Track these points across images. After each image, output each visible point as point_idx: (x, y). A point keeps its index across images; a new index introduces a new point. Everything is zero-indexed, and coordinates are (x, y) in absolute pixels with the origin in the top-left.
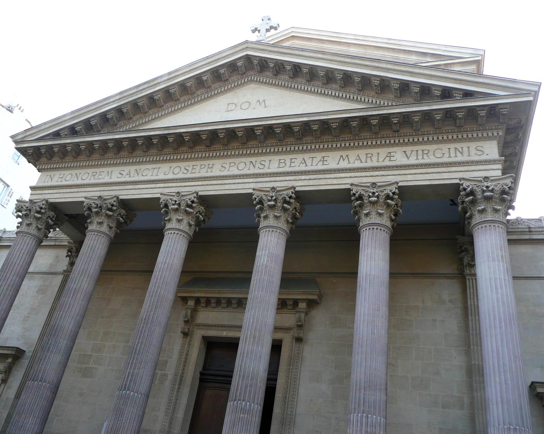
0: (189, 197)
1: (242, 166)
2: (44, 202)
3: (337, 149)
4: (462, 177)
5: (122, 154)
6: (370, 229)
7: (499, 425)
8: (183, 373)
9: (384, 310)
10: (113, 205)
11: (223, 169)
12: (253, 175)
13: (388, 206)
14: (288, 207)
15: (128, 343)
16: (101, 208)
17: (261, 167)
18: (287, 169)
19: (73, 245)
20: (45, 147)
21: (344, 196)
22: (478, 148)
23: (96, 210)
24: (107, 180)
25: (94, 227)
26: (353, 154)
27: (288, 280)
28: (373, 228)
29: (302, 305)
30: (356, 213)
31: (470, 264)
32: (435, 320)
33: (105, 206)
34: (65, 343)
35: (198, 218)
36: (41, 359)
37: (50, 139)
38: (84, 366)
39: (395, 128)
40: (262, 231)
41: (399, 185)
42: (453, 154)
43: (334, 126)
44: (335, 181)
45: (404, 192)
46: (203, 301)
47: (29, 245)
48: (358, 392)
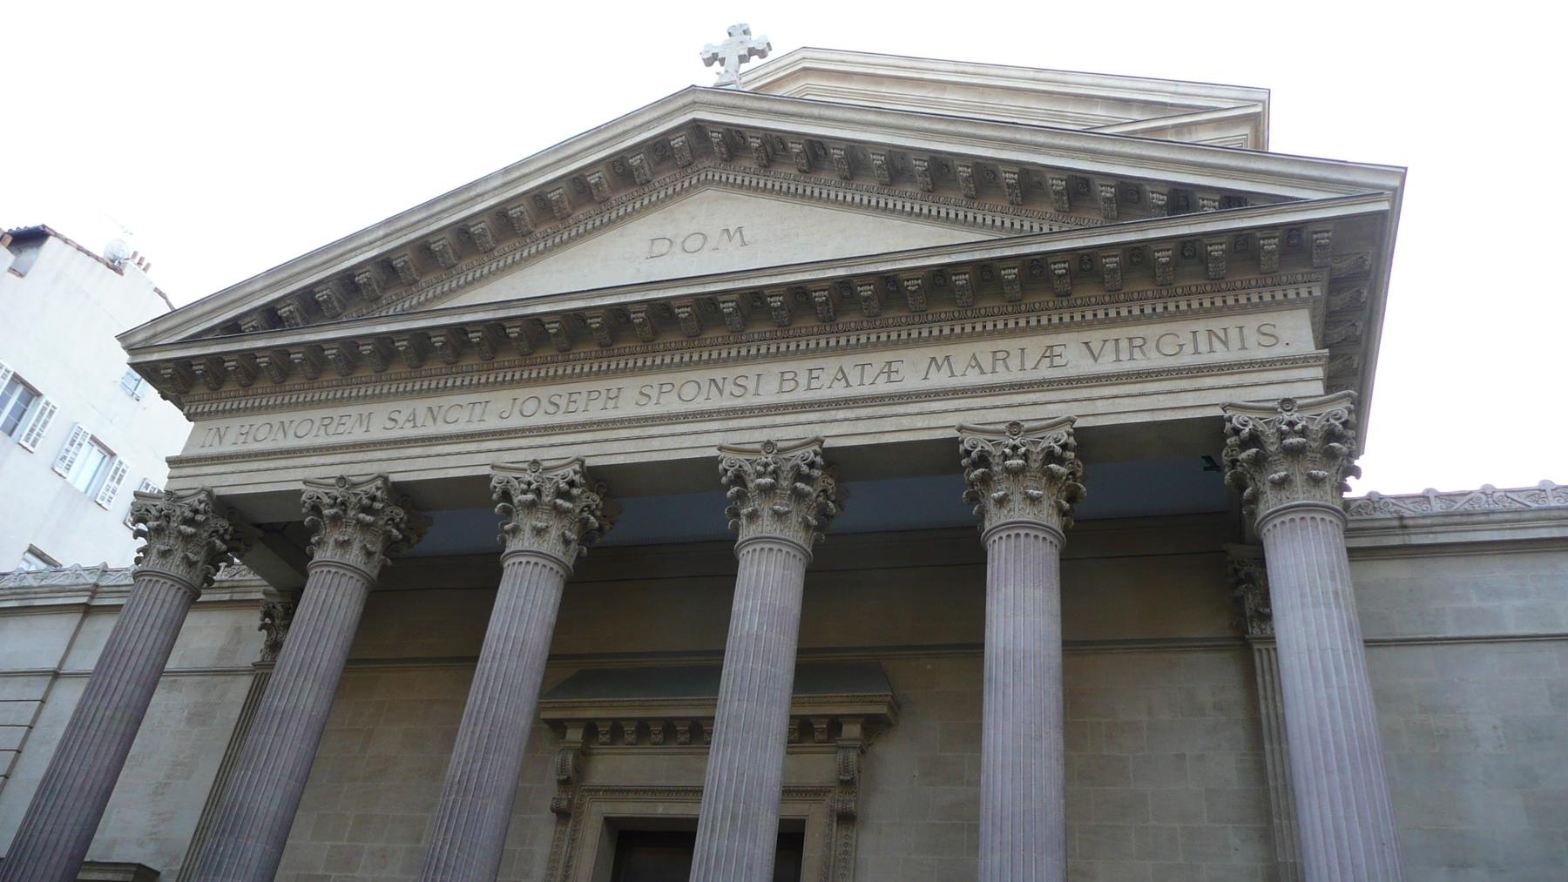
2: (202, 496)
3: (921, 342)
5: (395, 370)
6: (1027, 535)
9: (1052, 739)
10: (373, 498)
11: (644, 400)
12: (719, 412)
13: (1053, 478)
15: (418, 841)
16: (345, 505)
17: (738, 391)
19: (276, 600)
22: (1264, 329)
23: (332, 511)
24: (359, 435)
26: (960, 353)
27: (812, 669)
28: (1018, 535)
30: (974, 498)
32: (1181, 757)
33: (353, 500)
35: (584, 523)
37: (216, 341)
42: (1203, 347)
43: (912, 286)
44: (920, 422)
45: (1089, 442)
46: (629, 728)
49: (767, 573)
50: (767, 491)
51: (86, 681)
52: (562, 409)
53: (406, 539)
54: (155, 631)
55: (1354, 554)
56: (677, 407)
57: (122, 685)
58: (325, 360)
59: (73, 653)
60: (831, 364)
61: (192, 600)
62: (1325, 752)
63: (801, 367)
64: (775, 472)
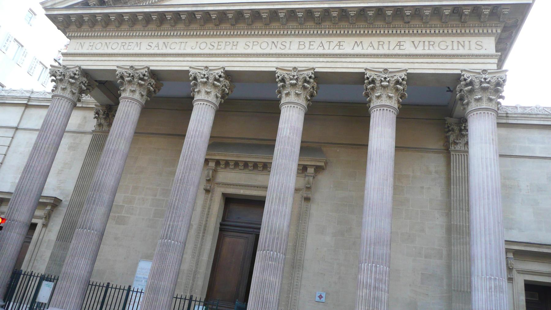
0: (217, 72)
1: (264, 45)
2: (77, 69)
3: (352, 35)
4: (464, 68)
5: (150, 26)
6: (387, 110)
7: (482, 275)
8: (206, 224)
9: (391, 180)
10: (144, 75)
11: (247, 47)
12: (276, 54)
13: (397, 90)
14: (308, 86)
15: (156, 196)
16: (133, 77)
17: (283, 47)
18: (306, 51)
19: (100, 108)
20: (75, 16)
21: (359, 78)
22: (478, 43)
23: (129, 79)
24: (136, 50)
25: (128, 94)
26: (366, 41)
27: (306, 148)
28: (383, 109)
29: (311, 170)
30: (367, 95)
31: (455, 142)
32: (422, 188)
33: (136, 75)
34: (108, 196)
35: (223, 91)
36: (88, 211)
37: (80, 8)
38: (117, 215)
39: (406, 19)
40: (284, 106)
41: (408, 72)
42: (455, 47)
43: (352, 14)
44: (350, 65)
45: (412, 78)
46: (232, 163)
47: (65, 108)
48: (368, 246)
49: (292, 115)
50: (205, 83)
51: (38, 132)
52: (216, 47)
53: (155, 91)
54: (62, 117)
55: (499, 125)
56: (260, 51)
57: (51, 136)
58: (96, 21)
59: (22, 121)
60: (318, 40)
61: (74, 106)
62: (483, 192)
63: (307, 40)
64: (297, 79)
